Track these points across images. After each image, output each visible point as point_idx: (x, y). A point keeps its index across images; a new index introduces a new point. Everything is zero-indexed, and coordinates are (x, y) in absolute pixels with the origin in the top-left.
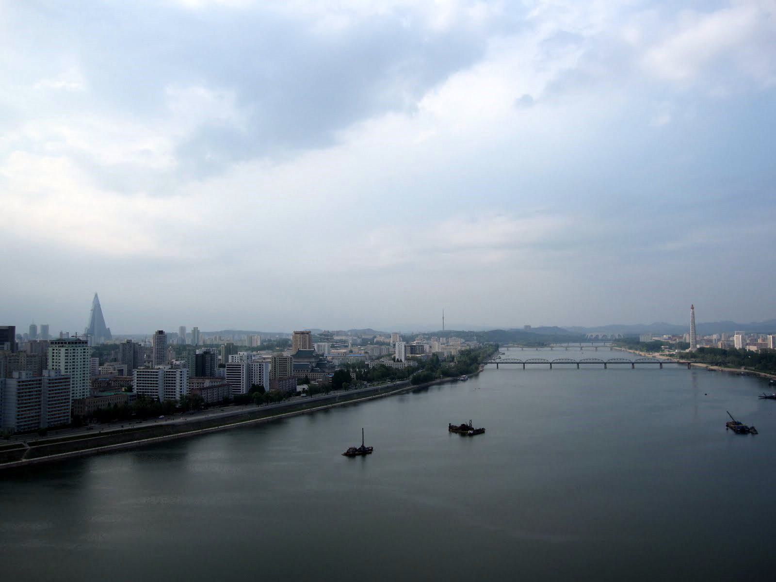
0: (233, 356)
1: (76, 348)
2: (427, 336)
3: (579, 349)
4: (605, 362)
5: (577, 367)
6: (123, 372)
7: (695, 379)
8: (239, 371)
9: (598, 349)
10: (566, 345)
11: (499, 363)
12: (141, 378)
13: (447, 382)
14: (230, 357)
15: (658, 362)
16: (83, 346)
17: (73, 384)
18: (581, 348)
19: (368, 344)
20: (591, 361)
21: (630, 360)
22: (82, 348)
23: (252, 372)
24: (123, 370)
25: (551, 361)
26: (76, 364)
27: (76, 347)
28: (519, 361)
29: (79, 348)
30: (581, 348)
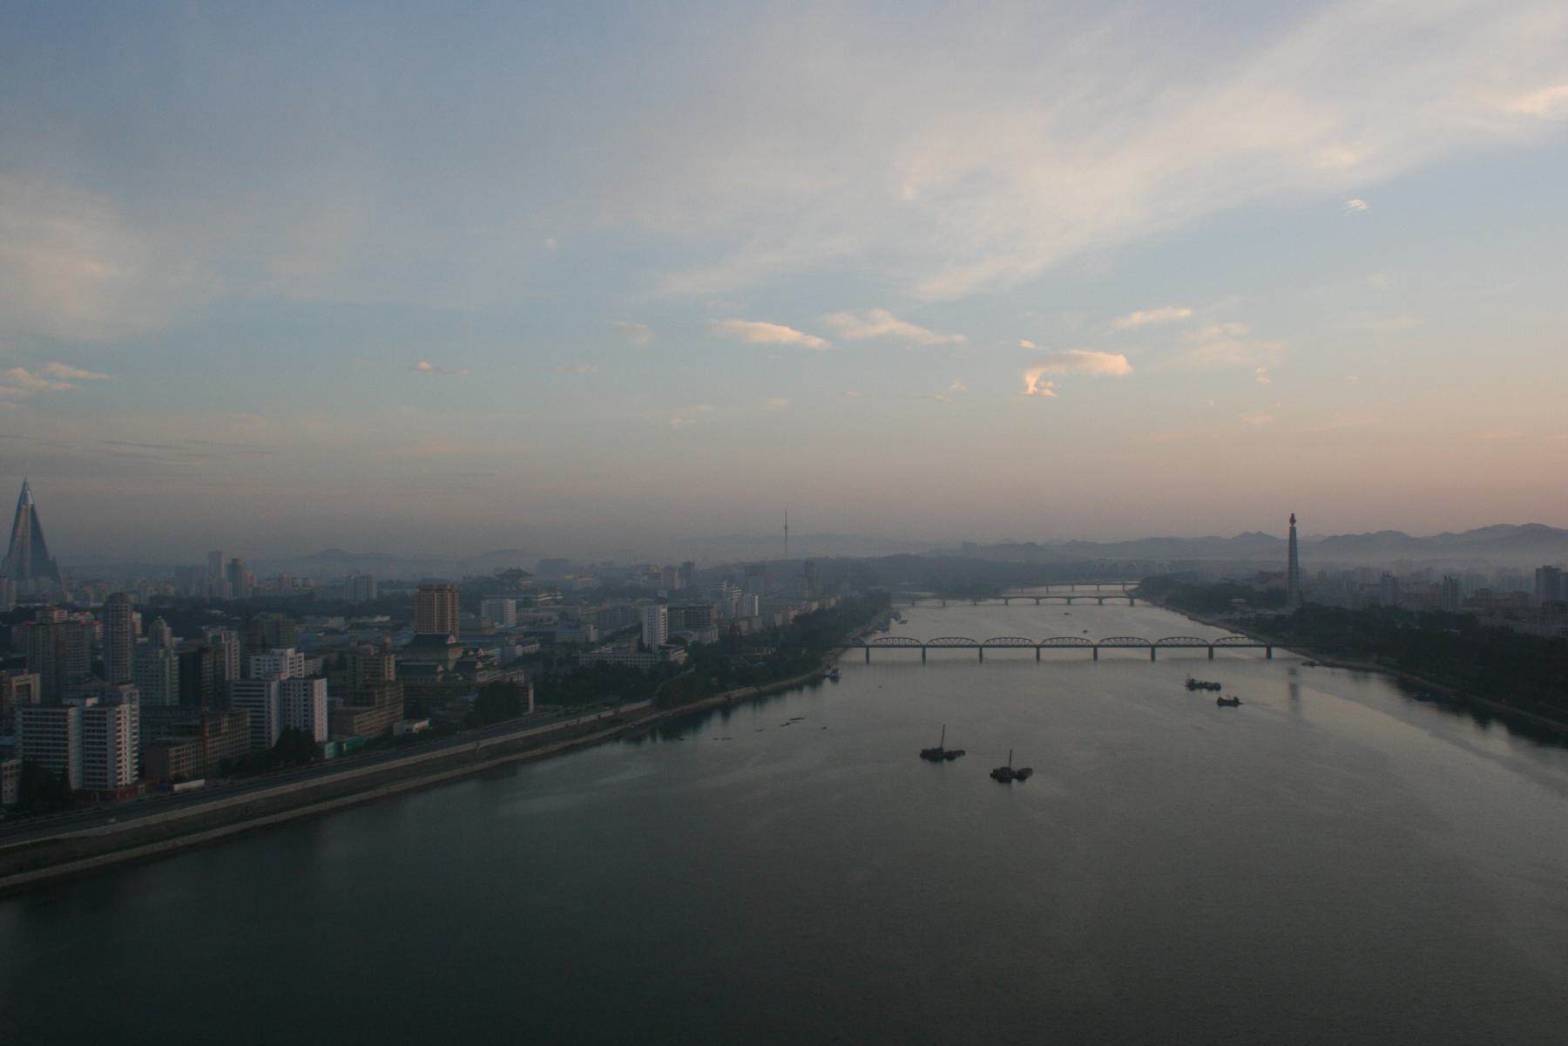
0: (260, 657)
2: (61, 773)
3: (1097, 601)
4: (1210, 643)
5: (1092, 657)
6: (29, 691)
7: (1294, 690)
8: (261, 698)
9: (1104, 601)
10: (1066, 590)
11: (984, 646)
12: (31, 726)
13: (744, 700)
14: (253, 659)
15: (1205, 643)
17: (300, 666)
18: (1101, 599)
19: (207, 738)
20: (1182, 642)
21: (1204, 641)
23: (289, 705)
24: (29, 686)
25: (1038, 642)
26: (271, 663)
28: (1200, 642)
30: (1101, 599)
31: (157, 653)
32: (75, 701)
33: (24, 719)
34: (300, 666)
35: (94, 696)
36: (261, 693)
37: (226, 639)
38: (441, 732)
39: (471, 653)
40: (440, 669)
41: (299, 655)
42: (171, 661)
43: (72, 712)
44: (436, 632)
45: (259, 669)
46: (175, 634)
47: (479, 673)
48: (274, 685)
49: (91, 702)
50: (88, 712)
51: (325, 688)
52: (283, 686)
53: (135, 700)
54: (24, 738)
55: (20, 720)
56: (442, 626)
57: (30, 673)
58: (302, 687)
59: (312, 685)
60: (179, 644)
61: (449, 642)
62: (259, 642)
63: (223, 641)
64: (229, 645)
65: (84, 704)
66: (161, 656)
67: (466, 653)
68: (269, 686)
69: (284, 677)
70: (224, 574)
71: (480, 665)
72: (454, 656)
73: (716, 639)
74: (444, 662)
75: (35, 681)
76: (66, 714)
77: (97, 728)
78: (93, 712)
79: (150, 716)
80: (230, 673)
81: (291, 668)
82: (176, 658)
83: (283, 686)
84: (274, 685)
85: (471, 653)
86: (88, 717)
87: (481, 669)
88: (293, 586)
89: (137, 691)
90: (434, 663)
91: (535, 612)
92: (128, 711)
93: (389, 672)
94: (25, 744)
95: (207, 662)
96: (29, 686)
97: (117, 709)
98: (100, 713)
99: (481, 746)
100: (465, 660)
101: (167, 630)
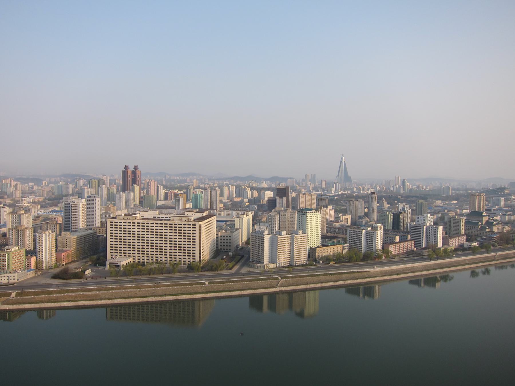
1: (312, 216)
22: (316, 215)
27: (312, 215)
29: (314, 216)
31: (387, 213)
32: (364, 228)
33: (350, 232)
34: (432, 219)
35: (370, 227)
36: (420, 238)
37: (406, 209)
38: (484, 247)
39: (491, 219)
40: (480, 223)
42: (390, 215)
43: (364, 231)
44: (477, 210)
45: (418, 222)
46: (388, 204)
47: (494, 226)
48: (425, 227)
49: (369, 229)
50: (368, 232)
51: (442, 229)
52: (428, 228)
53: (382, 229)
54: (350, 238)
56: (479, 207)
57: (348, 215)
59: (438, 228)
61: (479, 224)
62: (418, 211)
64: (408, 211)
65: (367, 229)
66: (388, 214)
67: (489, 219)
68: (423, 227)
69: (428, 225)
71: (494, 223)
72: (485, 219)
74: (482, 221)
75: (349, 217)
76: (362, 232)
77: (371, 237)
78: (370, 232)
79: (386, 231)
81: (429, 221)
82: (392, 215)
83: (427, 227)
84: (425, 227)
85: (491, 219)
86: (368, 233)
87: (495, 225)
89: (382, 226)
90: (477, 221)
91: (510, 202)
92: (380, 233)
93: (462, 227)
94: (350, 234)
95: (401, 216)
96: (348, 219)
97: (377, 232)
98: (372, 232)
99: (497, 255)
100: (489, 221)
101: (385, 203)
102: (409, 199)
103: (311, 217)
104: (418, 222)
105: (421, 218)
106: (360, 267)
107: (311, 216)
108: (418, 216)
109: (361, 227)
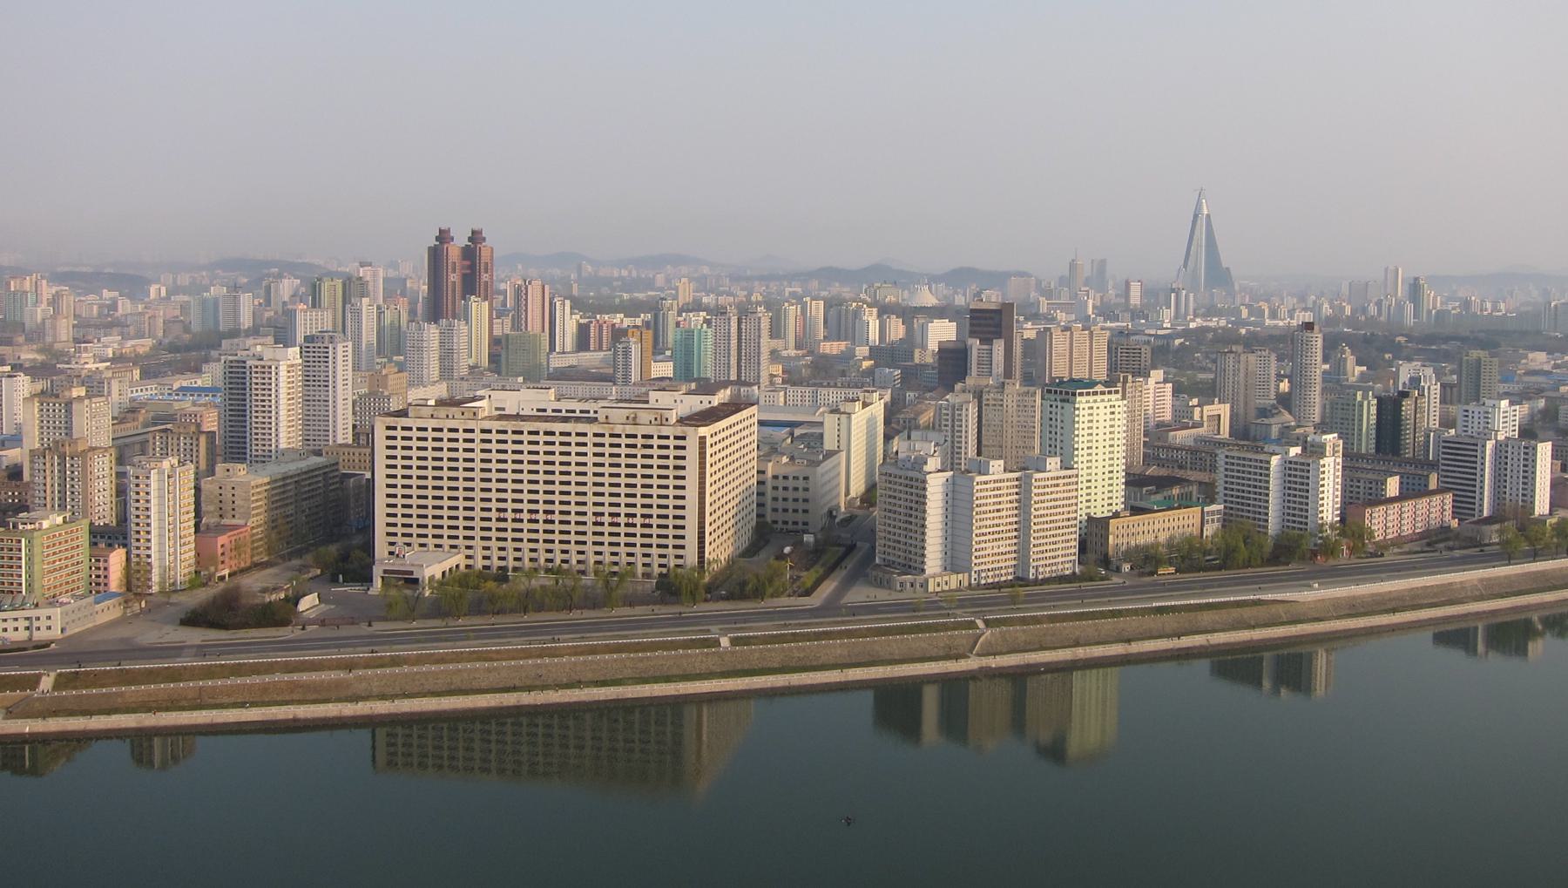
1: (1095, 405)
11: (186, 734)
16: (1110, 400)
22: (1108, 404)
27: (1095, 401)
29: (1102, 405)
31: (1355, 395)
32: (1277, 449)
35: (1297, 445)
41: (1513, 408)
43: (1275, 460)
45: (1467, 416)
46: (1359, 363)
48: (1490, 445)
49: (1295, 451)
50: (1290, 462)
53: (1338, 452)
55: (1222, 463)
57: (1220, 403)
58: (1482, 416)
59: (1535, 449)
60: (1362, 373)
63: (1422, 384)
64: (1429, 388)
65: (1287, 453)
66: (1359, 398)
68: (1484, 446)
69: (1501, 437)
70: (1401, 291)
73: (1530, 646)
75: (1224, 410)
76: (1268, 462)
77: (1300, 481)
78: (1296, 463)
80: (1428, 423)
82: (1375, 402)
83: (1499, 447)
84: (1490, 445)
86: (1288, 465)
88: (1481, 310)
89: (1341, 442)
94: (1226, 489)
95: (1407, 406)
96: (1219, 416)
98: (1303, 464)
101: (1351, 359)
102: (1434, 347)
103: (1089, 408)
104: (1467, 416)
105: (1476, 413)
106: (1261, 586)
107: (1092, 408)
108: (1466, 407)
109: (1266, 446)
